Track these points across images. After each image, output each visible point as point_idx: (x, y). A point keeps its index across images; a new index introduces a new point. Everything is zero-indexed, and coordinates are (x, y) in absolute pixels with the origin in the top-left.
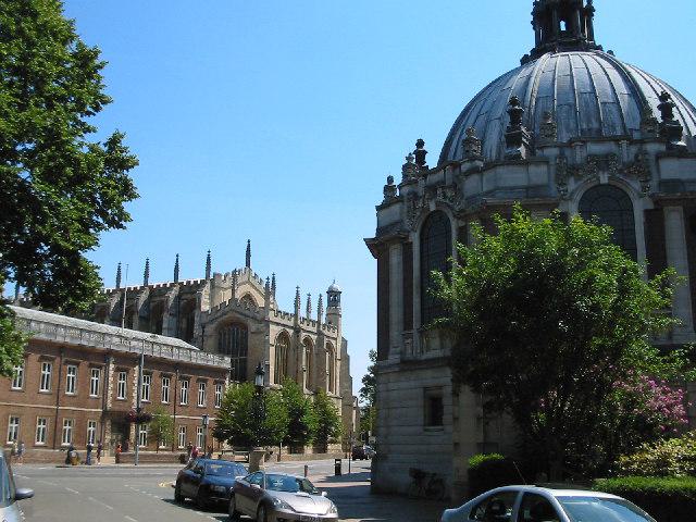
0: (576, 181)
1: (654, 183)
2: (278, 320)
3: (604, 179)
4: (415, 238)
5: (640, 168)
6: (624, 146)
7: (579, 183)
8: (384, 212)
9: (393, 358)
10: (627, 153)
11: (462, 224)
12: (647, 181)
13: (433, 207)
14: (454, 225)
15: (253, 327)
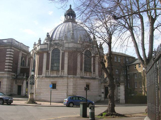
11: (63, 52)
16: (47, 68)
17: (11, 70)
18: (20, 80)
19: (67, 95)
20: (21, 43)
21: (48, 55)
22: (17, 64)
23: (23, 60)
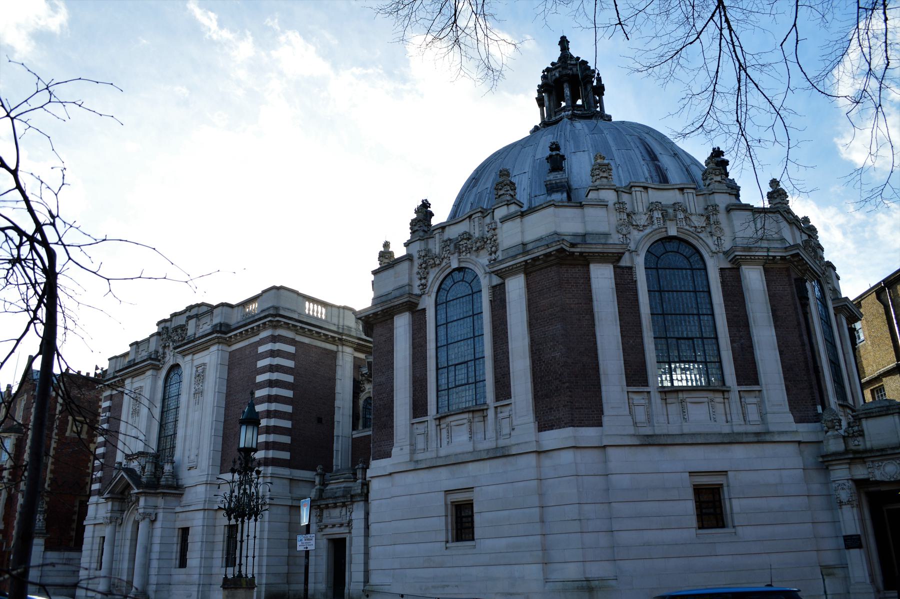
11: (496, 281)
16: (419, 408)
17: (286, 455)
18: (335, 506)
19: (546, 581)
20: (345, 308)
21: (418, 316)
22: (326, 420)
23: (363, 396)
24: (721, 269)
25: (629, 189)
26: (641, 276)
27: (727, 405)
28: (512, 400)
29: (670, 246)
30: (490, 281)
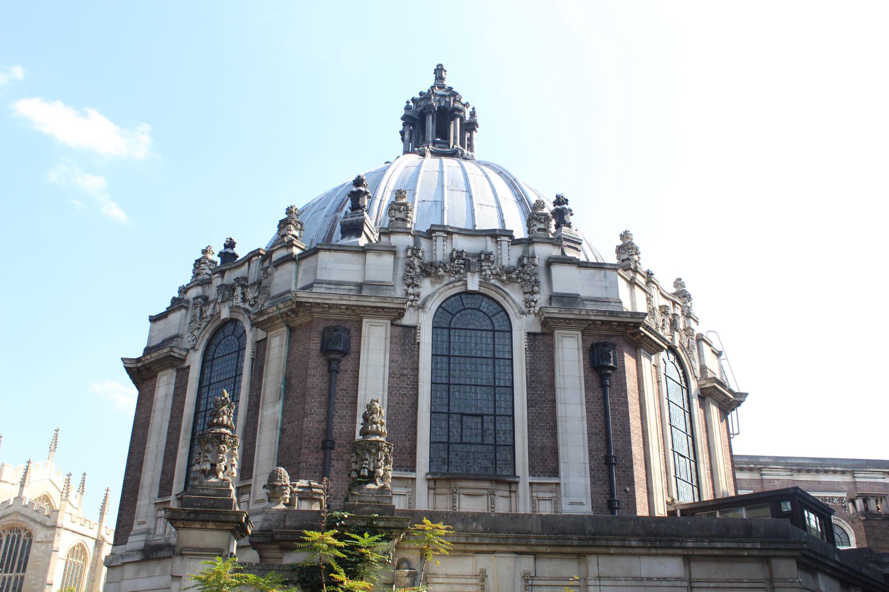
0: (433, 283)
1: (541, 298)
2: (76, 527)
3: (473, 283)
4: (195, 361)
5: (523, 274)
6: (505, 244)
7: (438, 286)
8: (161, 324)
9: (136, 542)
10: (509, 256)
11: (261, 335)
12: (533, 293)
13: (225, 314)
14: (251, 337)
15: (40, 534)
24: (529, 334)
25: (430, 234)
26: (426, 337)
27: (513, 500)
28: (252, 481)
29: (468, 301)
30: (255, 335)
